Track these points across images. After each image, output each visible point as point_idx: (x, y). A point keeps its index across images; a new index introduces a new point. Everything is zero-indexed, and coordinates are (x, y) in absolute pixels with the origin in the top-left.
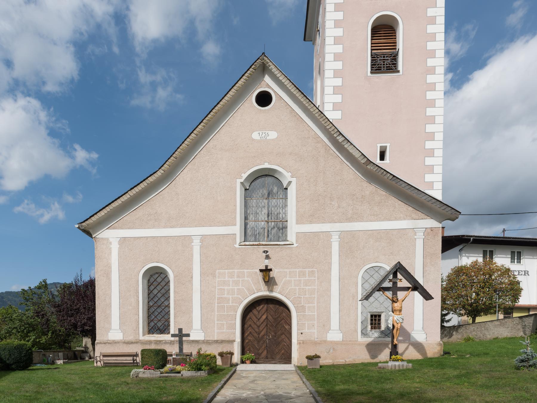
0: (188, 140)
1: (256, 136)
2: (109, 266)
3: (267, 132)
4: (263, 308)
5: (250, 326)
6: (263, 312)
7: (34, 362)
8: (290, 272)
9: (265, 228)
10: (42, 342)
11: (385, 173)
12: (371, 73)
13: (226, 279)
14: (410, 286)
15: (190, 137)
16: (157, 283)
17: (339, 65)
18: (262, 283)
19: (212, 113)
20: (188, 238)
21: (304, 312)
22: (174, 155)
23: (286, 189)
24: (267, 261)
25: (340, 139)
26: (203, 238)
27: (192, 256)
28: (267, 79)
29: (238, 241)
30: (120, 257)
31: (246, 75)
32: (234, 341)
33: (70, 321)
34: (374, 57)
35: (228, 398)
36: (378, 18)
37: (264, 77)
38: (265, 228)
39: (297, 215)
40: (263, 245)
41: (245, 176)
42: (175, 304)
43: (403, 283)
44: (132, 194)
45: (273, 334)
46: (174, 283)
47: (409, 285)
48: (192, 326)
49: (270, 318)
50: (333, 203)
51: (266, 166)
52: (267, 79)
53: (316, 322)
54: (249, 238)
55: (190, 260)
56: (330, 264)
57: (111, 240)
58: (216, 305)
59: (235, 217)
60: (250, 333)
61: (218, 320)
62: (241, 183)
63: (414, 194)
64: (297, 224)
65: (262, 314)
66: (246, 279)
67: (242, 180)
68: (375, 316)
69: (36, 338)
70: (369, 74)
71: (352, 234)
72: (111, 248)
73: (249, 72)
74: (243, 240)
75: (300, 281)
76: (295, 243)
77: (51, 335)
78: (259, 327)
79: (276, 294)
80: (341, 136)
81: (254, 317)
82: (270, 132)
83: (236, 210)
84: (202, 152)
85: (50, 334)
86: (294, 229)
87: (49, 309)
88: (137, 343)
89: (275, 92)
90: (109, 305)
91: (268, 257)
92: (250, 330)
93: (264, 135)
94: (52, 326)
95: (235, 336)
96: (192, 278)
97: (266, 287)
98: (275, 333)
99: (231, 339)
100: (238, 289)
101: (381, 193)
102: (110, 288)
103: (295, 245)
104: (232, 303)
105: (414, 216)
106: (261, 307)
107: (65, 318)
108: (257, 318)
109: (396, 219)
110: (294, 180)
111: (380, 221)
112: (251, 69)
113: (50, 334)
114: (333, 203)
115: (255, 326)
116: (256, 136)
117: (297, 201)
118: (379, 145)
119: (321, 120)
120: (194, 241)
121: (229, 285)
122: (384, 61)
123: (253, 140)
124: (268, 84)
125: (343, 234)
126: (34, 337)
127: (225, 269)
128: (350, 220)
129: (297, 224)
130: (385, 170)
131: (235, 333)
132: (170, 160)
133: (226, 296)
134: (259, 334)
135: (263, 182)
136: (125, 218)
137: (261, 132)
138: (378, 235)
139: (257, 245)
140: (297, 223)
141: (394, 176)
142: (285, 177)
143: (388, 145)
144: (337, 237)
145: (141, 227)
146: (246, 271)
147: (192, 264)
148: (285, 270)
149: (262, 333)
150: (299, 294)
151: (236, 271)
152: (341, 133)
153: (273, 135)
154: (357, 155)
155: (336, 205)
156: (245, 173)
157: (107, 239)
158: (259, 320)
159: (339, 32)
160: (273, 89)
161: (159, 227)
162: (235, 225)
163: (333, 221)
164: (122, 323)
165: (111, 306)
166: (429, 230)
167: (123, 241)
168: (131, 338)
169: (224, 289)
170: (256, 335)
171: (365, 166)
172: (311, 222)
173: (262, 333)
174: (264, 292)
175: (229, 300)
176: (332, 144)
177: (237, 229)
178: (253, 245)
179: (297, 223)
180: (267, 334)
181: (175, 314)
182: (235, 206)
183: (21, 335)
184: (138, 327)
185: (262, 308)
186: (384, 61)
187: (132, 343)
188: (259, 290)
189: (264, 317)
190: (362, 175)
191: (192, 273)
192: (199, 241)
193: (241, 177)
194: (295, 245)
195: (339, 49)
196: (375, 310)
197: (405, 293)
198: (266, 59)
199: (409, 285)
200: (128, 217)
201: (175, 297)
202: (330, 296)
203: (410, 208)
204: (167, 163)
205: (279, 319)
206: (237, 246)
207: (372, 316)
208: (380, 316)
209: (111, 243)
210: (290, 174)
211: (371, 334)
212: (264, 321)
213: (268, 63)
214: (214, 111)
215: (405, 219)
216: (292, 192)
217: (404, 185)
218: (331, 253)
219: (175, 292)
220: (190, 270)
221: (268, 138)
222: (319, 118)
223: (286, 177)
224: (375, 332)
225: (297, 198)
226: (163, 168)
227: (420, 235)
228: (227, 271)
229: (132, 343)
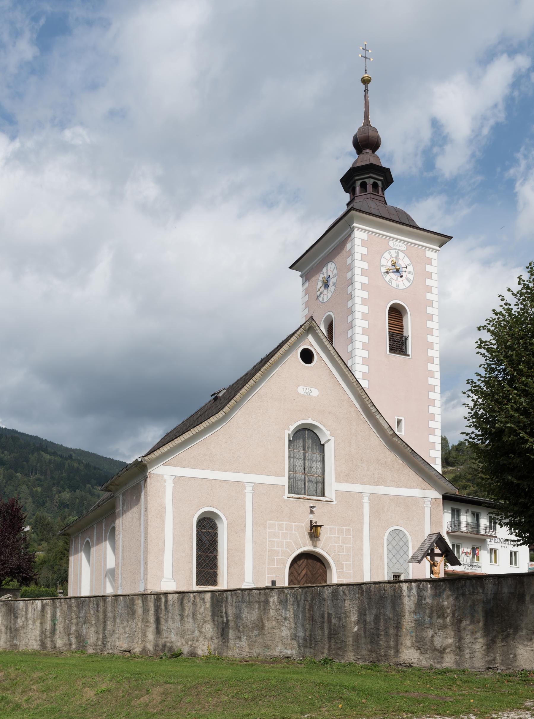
2: (163, 507)
3: (310, 388)
4: (303, 563)
6: (303, 567)
8: (330, 528)
9: (307, 483)
11: (406, 446)
18: (307, 538)
20: (242, 484)
21: (343, 569)
24: (311, 515)
25: (373, 410)
26: (256, 485)
27: (245, 504)
28: (310, 338)
30: (174, 497)
36: (393, 304)
37: (308, 336)
38: (307, 483)
39: (336, 473)
40: (308, 499)
42: (228, 554)
46: (228, 531)
48: (244, 579)
51: (310, 421)
52: (310, 338)
56: (362, 523)
57: (165, 477)
58: (267, 557)
59: (284, 468)
61: (268, 574)
63: (426, 468)
64: (335, 482)
70: (388, 352)
72: (165, 486)
75: (339, 538)
76: (334, 501)
79: (318, 550)
80: (374, 407)
81: (295, 572)
82: (313, 389)
83: (284, 461)
84: (254, 398)
86: (333, 487)
91: (312, 512)
93: (307, 391)
96: (245, 527)
97: (311, 542)
104: (281, 556)
105: (423, 486)
106: (302, 561)
108: (297, 573)
109: (411, 487)
116: (300, 390)
117: (336, 460)
119: (358, 389)
120: (247, 488)
122: (398, 344)
123: (299, 394)
127: (275, 521)
128: (376, 483)
130: (406, 444)
133: (276, 548)
135: (306, 437)
136: (180, 456)
141: (413, 450)
142: (324, 434)
143: (403, 419)
145: (196, 467)
146: (293, 524)
151: (285, 523)
153: (315, 392)
154: (386, 426)
156: (292, 425)
157: (162, 476)
158: (299, 575)
162: (284, 476)
163: (363, 483)
164: (175, 572)
165: (164, 551)
166: (434, 500)
167: (178, 479)
169: (274, 541)
171: (391, 437)
172: (347, 482)
174: (308, 548)
175: (279, 553)
176: (363, 411)
177: (285, 481)
182: (284, 456)
186: (398, 344)
188: (305, 545)
189: (304, 572)
190: (386, 443)
191: (244, 521)
193: (289, 429)
194: (335, 503)
196: (397, 571)
198: (313, 322)
200: (183, 454)
203: (420, 479)
205: (317, 575)
207: (394, 576)
209: (165, 481)
215: (416, 488)
216: (330, 451)
217: (420, 459)
218: (363, 513)
220: (243, 518)
221: (311, 394)
222: (356, 387)
227: (428, 504)
228: (276, 522)
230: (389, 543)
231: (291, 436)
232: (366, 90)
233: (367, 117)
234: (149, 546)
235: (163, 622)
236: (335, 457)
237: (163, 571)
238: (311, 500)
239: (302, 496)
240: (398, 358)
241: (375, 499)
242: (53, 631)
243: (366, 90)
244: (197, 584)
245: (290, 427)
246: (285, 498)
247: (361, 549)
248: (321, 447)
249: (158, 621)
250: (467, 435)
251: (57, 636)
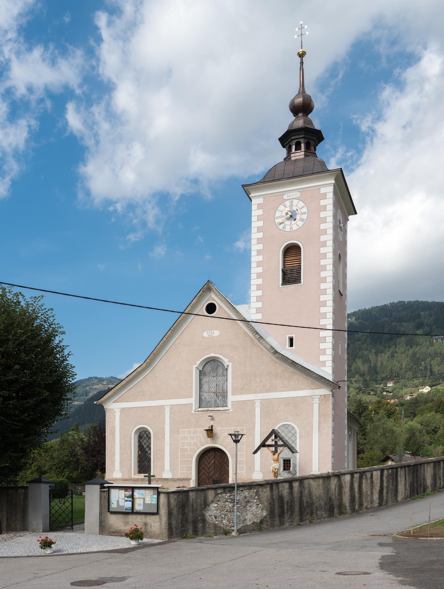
0: (162, 342)
1: (205, 334)
2: (114, 428)
5: (203, 468)
8: (227, 429)
9: (211, 397)
10: (73, 476)
12: (282, 285)
13: (186, 435)
15: (163, 340)
16: (144, 439)
17: (260, 281)
19: (176, 323)
20: (162, 408)
22: (153, 353)
23: (227, 369)
24: (212, 422)
26: (172, 407)
29: (194, 408)
31: (198, 296)
32: (191, 479)
33: (93, 461)
34: (284, 273)
38: (211, 397)
41: (198, 363)
44: (127, 380)
45: (218, 473)
48: (164, 469)
49: (217, 462)
50: (256, 379)
51: (212, 355)
53: (245, 465)
54: (203, 405)
55: (163, 422)
56: (254, 423)
57: (115, 410)
60: (204, 473)
62: (196, 368)
64: (232, 395)
65: (211, 460)
66: (199, 435)
67: (196, 366)
68: (287, 460)
69: (69, 473)
70: (280, 286)
71: (269, 401)
73: (199, 294)
74: (198, 407)
77: (81, 470)
78: (209, 468)
82: (215, 331)
83: (192, 387)
84: (171, 347)
85: (80, 470)
86: (231, 398)
87: (79, 450)
88: (130, 480)
89: (218, 303)
90: (114, 455)
91: (213, 419)
92: (203, 471)
94: (81, 463)
95: (191, 476)
98: (220, 473)
99: (189, 478)
100: (193, 442)
101: (290, 369)
102: (114, 443)
103: (231, 410)
107: (90, 458)
109: (300, 389)
110: (230, 364)
111: (288, 391)
112: (201, 292)
113: (80, 470)
114: (256, 379)
115: (207, 468)
116: (205, 334)
118: (288, 336)
120: (166, 409)
121: (188, 440)
122: (291, 276)
123: (204, 337)
124: (213, 298)
125: (263, 401)
126: (68, 473)
128: (268, 391)
129: (232, 395)
131: (191, 474)
132: (150, 356)
134: (209, 474)
135: (211, 367)
137: (209, 332)
138: (287, 401)
139: (206, 411)
140: (233, 394)
144: (259, 403)
145: (134, 400)
146: (198, 429)
147: (165, 425)
148: (224, 428)
149: (212, 473)
151: (192, 429)
152: (257, 333)
155: (259, 380)
157: (113, 409)
159: (260, 258)
160: (216, 302)
161: (144, 400)
162: (192, 397)
164: (121, 467)
166: (323, 397)
167: (123, 410)
168: (126, 477)
169: (185, 442)
170: (207, 474)
172: (242, 394)
173: (212, 473)
174: (209, 444)
177: (193, 400)
178: (203, 411)
179: (233, 394)
180: (214, 474)
181: (154, 460)
182: (192, 384)
183: (58, 471)
184: (131, 469)
185: (211, 454)
186: (291, 276)
187: (127, 480)
189: (213, 461)
191: (164, 431)
192: (169, 409)
193: (196, 364)
194: (231, 410)
195: (260, 270)
196: (285, 457)
197: (282, 448)
199: (282, 443)
201: (154, 448)
204: (149, 358)
206: (193, 412)
207: (284, 461)
208: (290, 460)
209: (115, 412)
210: (228, 360)
211: (282, 474)
212: (212, 464)
213: (211, 287)
214: (178, 321)
218: (255, 415)
219: (153, 444)
220: (163, 429)
221: (213, 335)
223: (226, 361)
224: (285, 472)
225: (232, 377)
226: (146, 362)
229: (127, 480)
232: (302, 63)
233: (302, 85)
243: (302, 63)
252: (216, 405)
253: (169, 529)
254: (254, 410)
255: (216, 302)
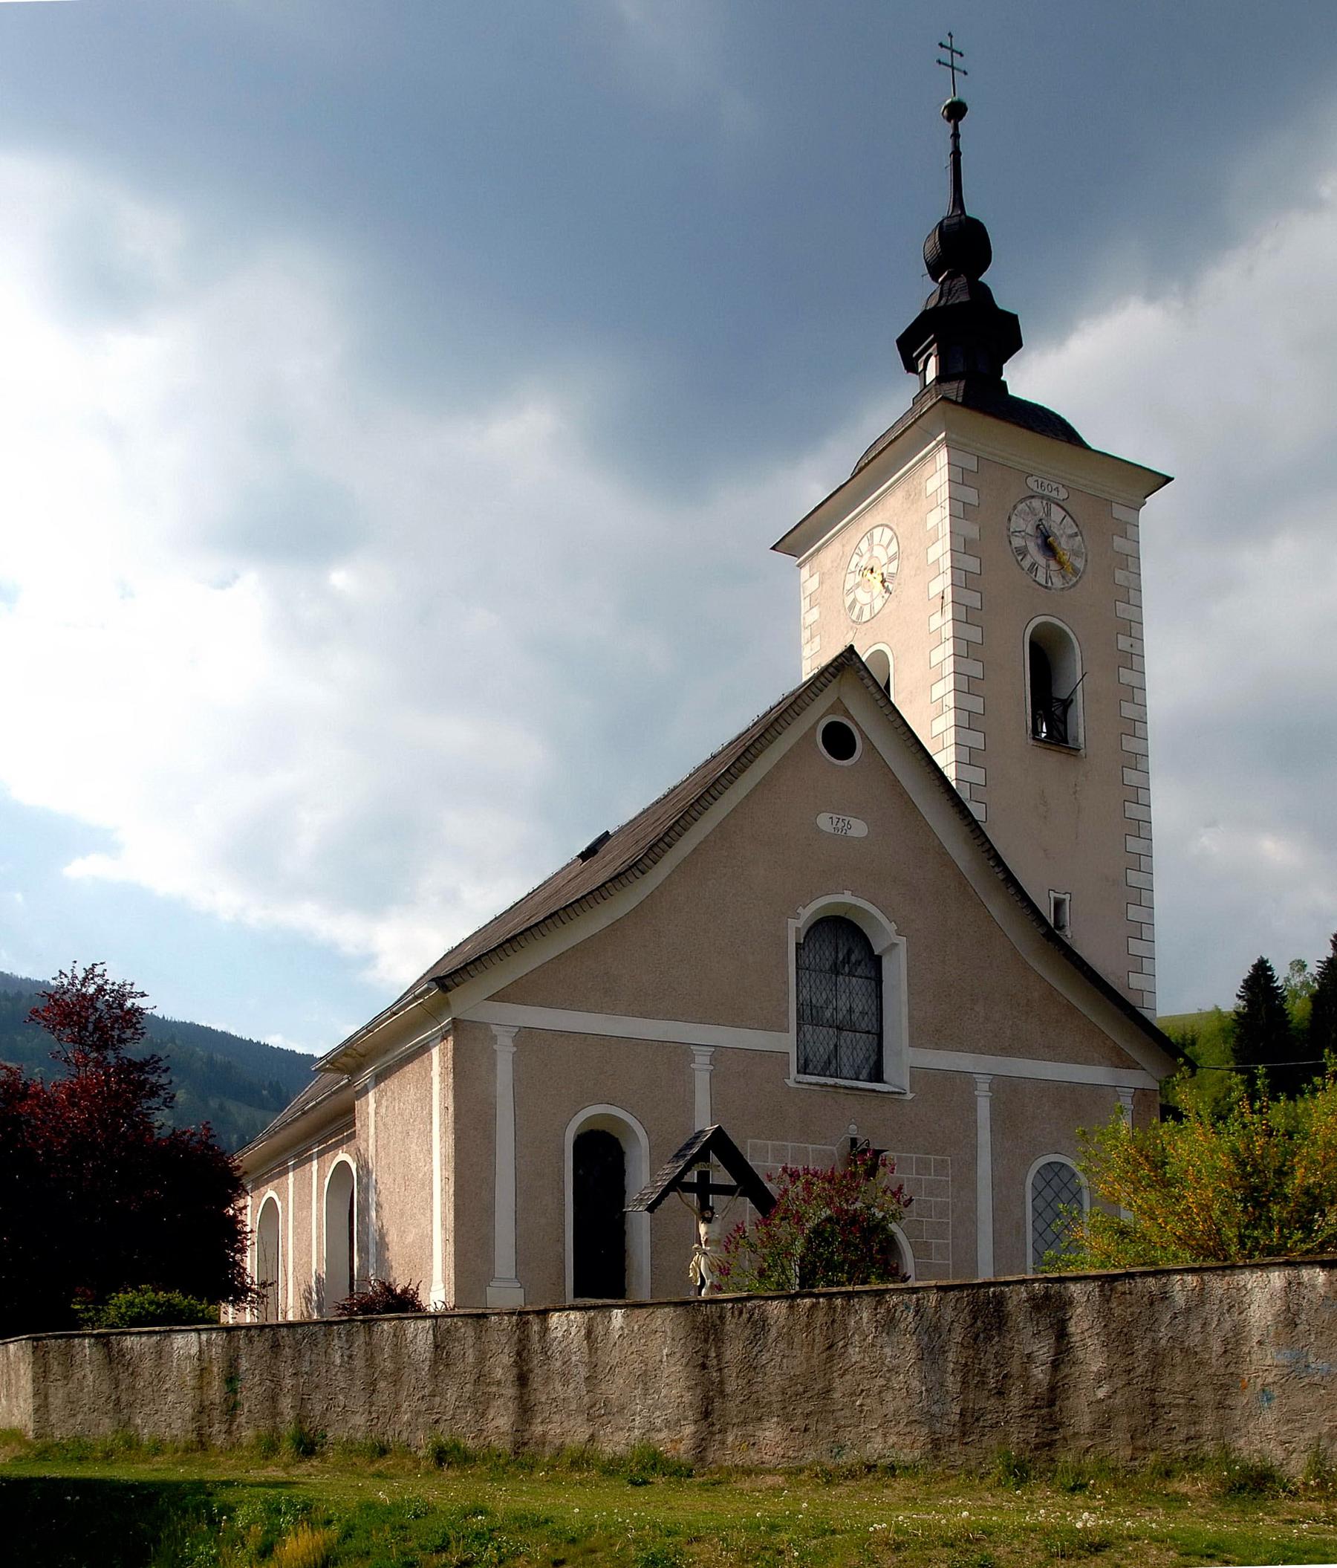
7: (243, 1159)
8: (899, 1158)
14: (734, 1183)
20: (683, 1051)
26: (719, 1054)
35: (688, 1397)
43: (720, 1176)
47: (686, 1179)
103: (910, 1096)
109: (1087, 1061)
116: (824, 822)
123: (819, 831)
128: (1007, 1051)
150: (918, 1215)
151: (790, 1144)
153: (859, 829)
157: (486, 1026)
160: (857, 725)
178: (825, 1085)
182: (786, 983)
199: (686, 1179)
202: (975, 1223)
209: (494, 1039)
210: (894, 926)
216: (896, 972)
218: (976, 1122)
221: (850, 833)
227: (1127, 1102)
230: (1038, 1194)
231: (803, 933)
232: (956, 136)
233: (958, 201)
234: (661, 830)
235: (536, 1381)
236: (909, 985)
237: (491, 1261)
238: (852, 1088)
239: (831, 1081)
240: (1052, 759)
241: (1006, 1090)
242: (232, 1409)
243: (956, 136)
244: (576, 1296)
245: (800, 910)
246: (791, 1083)
247: (972, 1209)
248: (877, 962)
249: (523, 1380)
250: (601, 1271)
251: (242, 1419)
252: (832, 1068)
253: (36, 1411)
254: (973, 1108)
255: (857, 725)
